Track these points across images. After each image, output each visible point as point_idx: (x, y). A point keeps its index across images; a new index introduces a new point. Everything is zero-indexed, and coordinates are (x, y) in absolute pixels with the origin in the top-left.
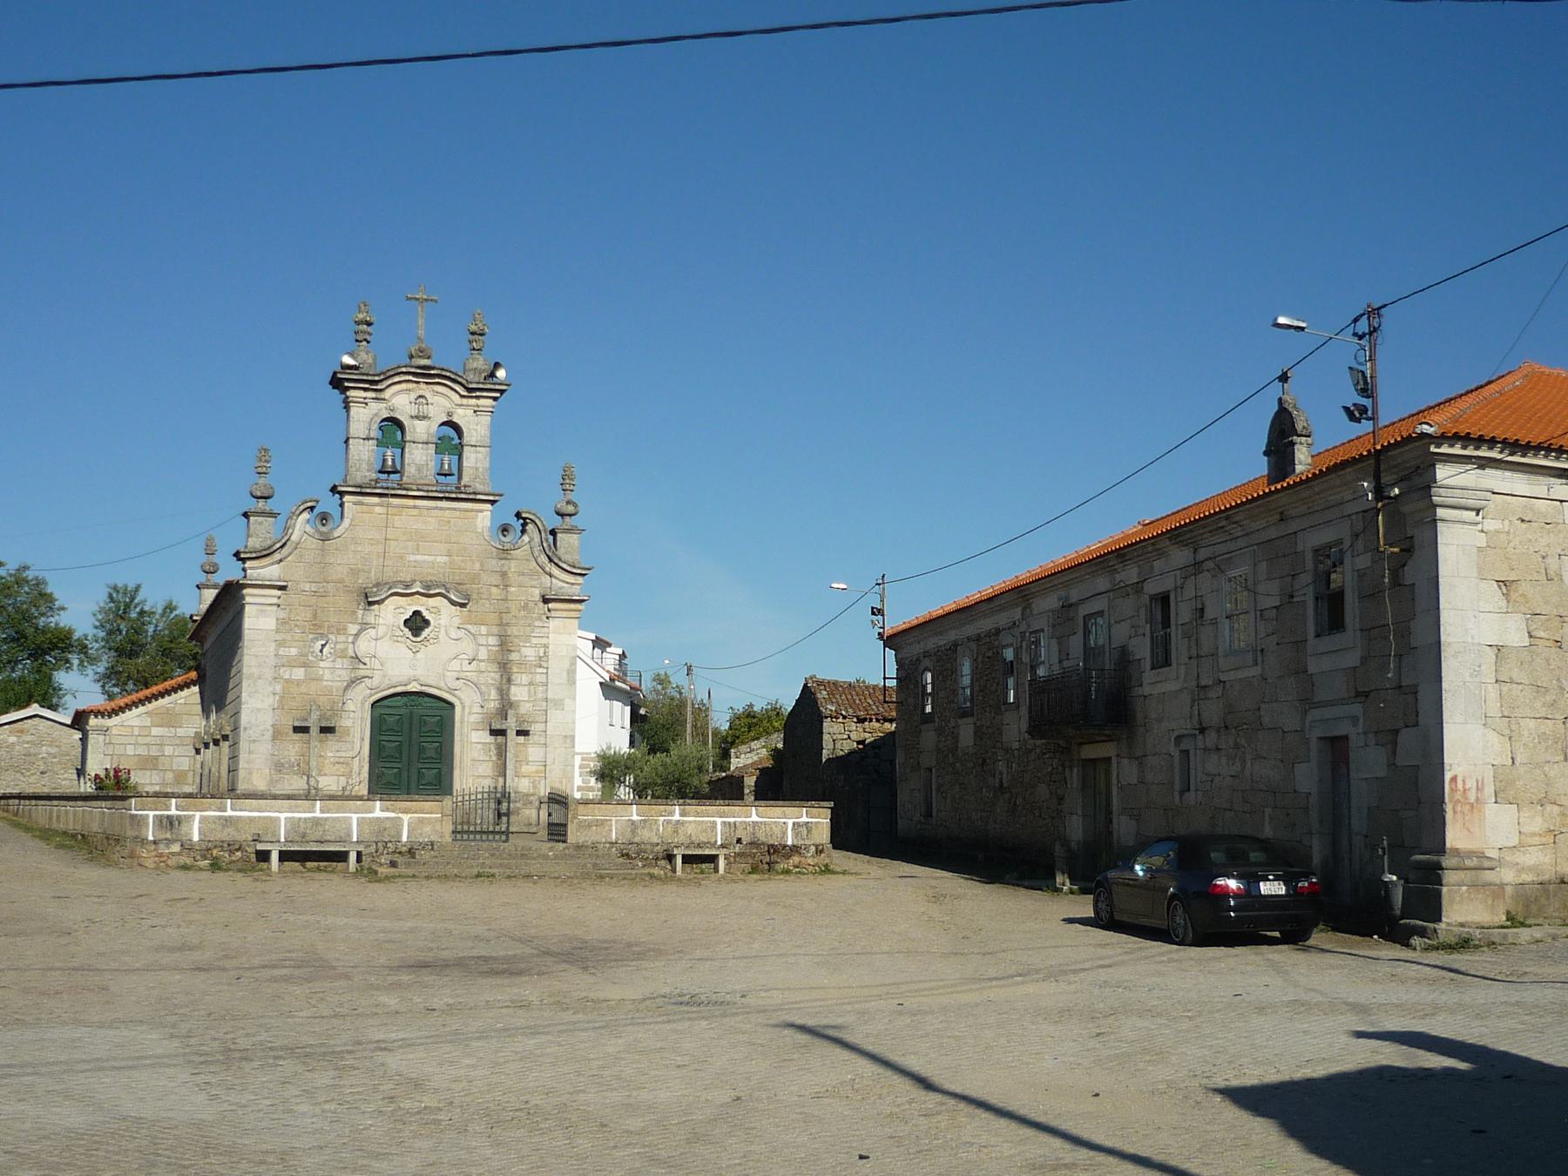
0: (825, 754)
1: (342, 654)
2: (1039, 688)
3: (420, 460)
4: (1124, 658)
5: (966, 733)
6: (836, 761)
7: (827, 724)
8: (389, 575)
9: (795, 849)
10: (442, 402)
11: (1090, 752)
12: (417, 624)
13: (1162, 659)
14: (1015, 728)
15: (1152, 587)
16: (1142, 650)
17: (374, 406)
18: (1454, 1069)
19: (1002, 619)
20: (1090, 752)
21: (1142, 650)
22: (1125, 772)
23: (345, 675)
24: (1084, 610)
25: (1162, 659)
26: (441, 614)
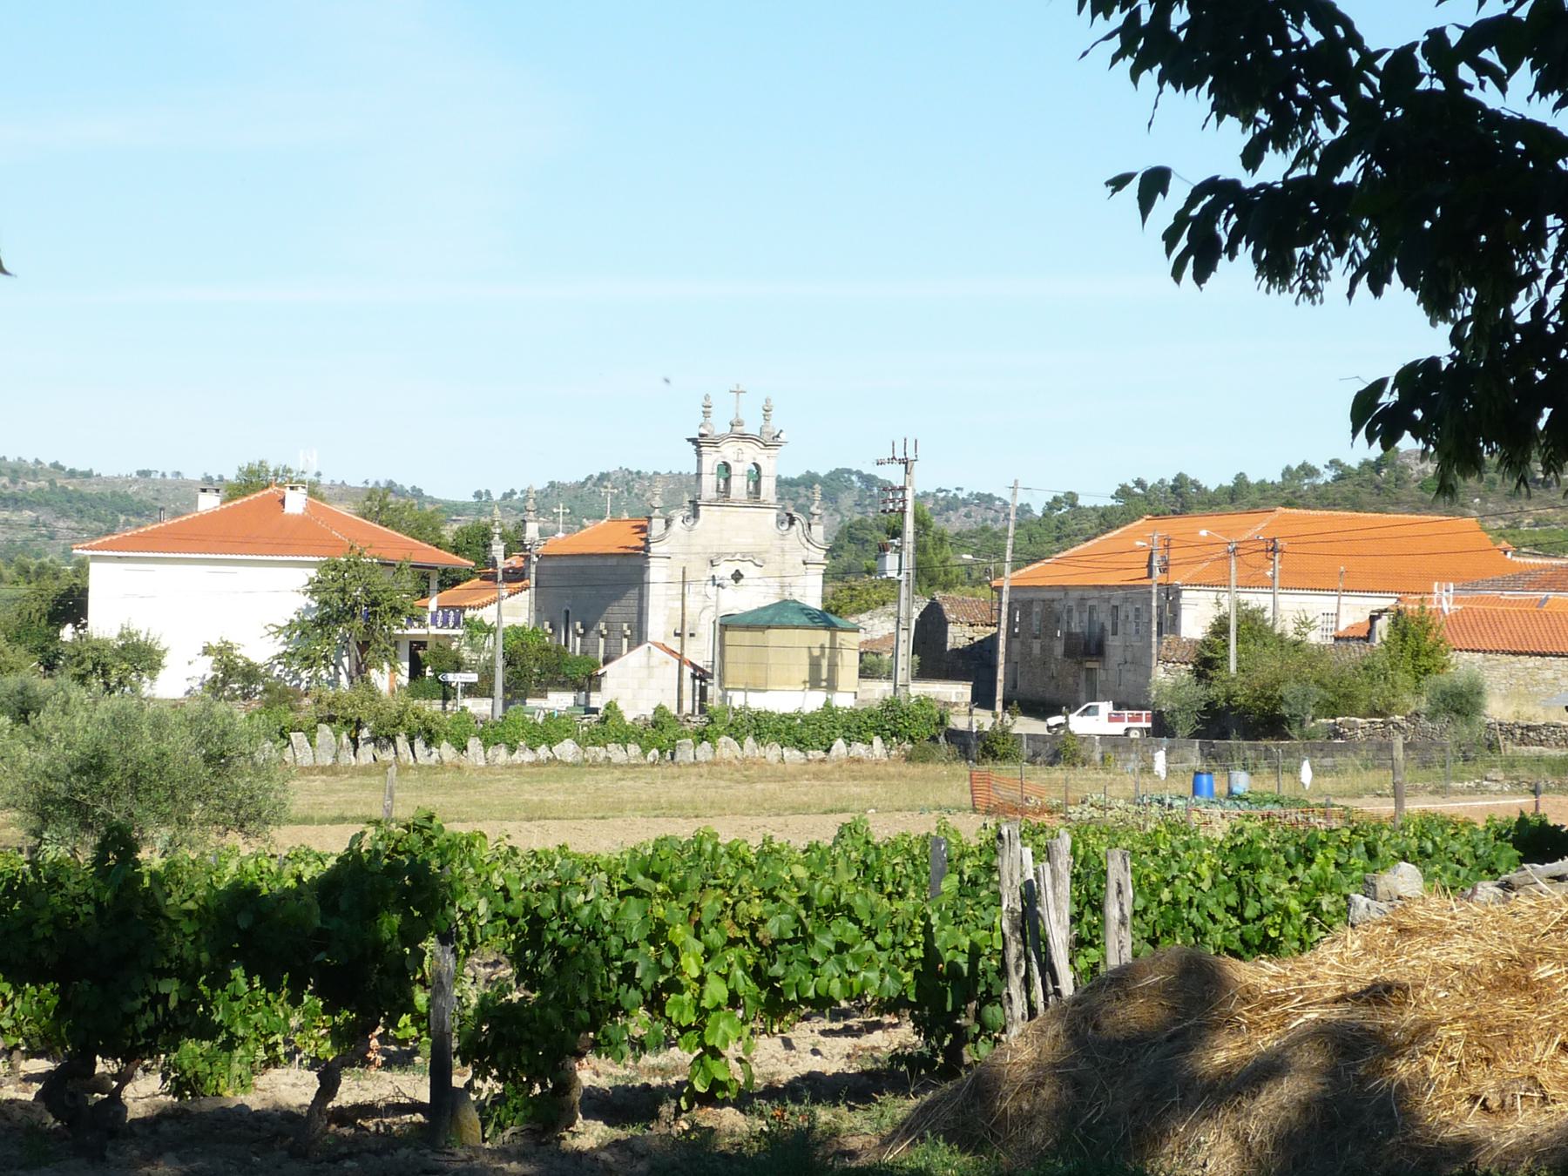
0: (949, 646)
1: (699, 593)
2: (1069, 636)
3: (739, 485)
4: (1103, 628)
5: (1036, 647)
6: (957, 652)
7: (950, 627)
8: (723, 550)
9: (956, 704)
10: (751, 453)
11: (1089, 665)
12: (737, 576)
13: (1115, 633)
14: (1059, 649)
15: (1113, 602)
16: (1109, 627)
17: (716, 455)
18: (994, 695)
19: (1056, 595)
20: (1089, 665)
21: (1109, 627)
22: (1101, 675)
23: (701, 606)
24: (1090, 603)
25: (1115, 633)
26: (748, 570)
